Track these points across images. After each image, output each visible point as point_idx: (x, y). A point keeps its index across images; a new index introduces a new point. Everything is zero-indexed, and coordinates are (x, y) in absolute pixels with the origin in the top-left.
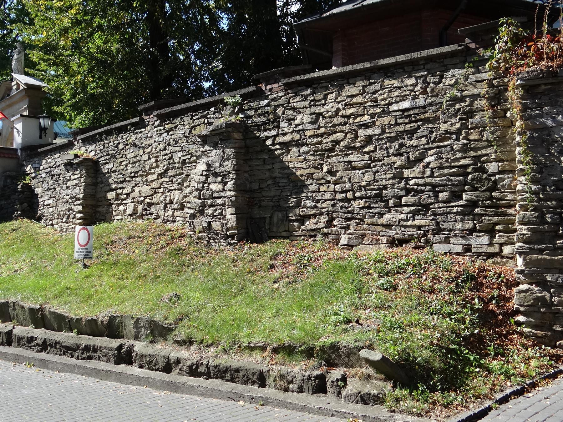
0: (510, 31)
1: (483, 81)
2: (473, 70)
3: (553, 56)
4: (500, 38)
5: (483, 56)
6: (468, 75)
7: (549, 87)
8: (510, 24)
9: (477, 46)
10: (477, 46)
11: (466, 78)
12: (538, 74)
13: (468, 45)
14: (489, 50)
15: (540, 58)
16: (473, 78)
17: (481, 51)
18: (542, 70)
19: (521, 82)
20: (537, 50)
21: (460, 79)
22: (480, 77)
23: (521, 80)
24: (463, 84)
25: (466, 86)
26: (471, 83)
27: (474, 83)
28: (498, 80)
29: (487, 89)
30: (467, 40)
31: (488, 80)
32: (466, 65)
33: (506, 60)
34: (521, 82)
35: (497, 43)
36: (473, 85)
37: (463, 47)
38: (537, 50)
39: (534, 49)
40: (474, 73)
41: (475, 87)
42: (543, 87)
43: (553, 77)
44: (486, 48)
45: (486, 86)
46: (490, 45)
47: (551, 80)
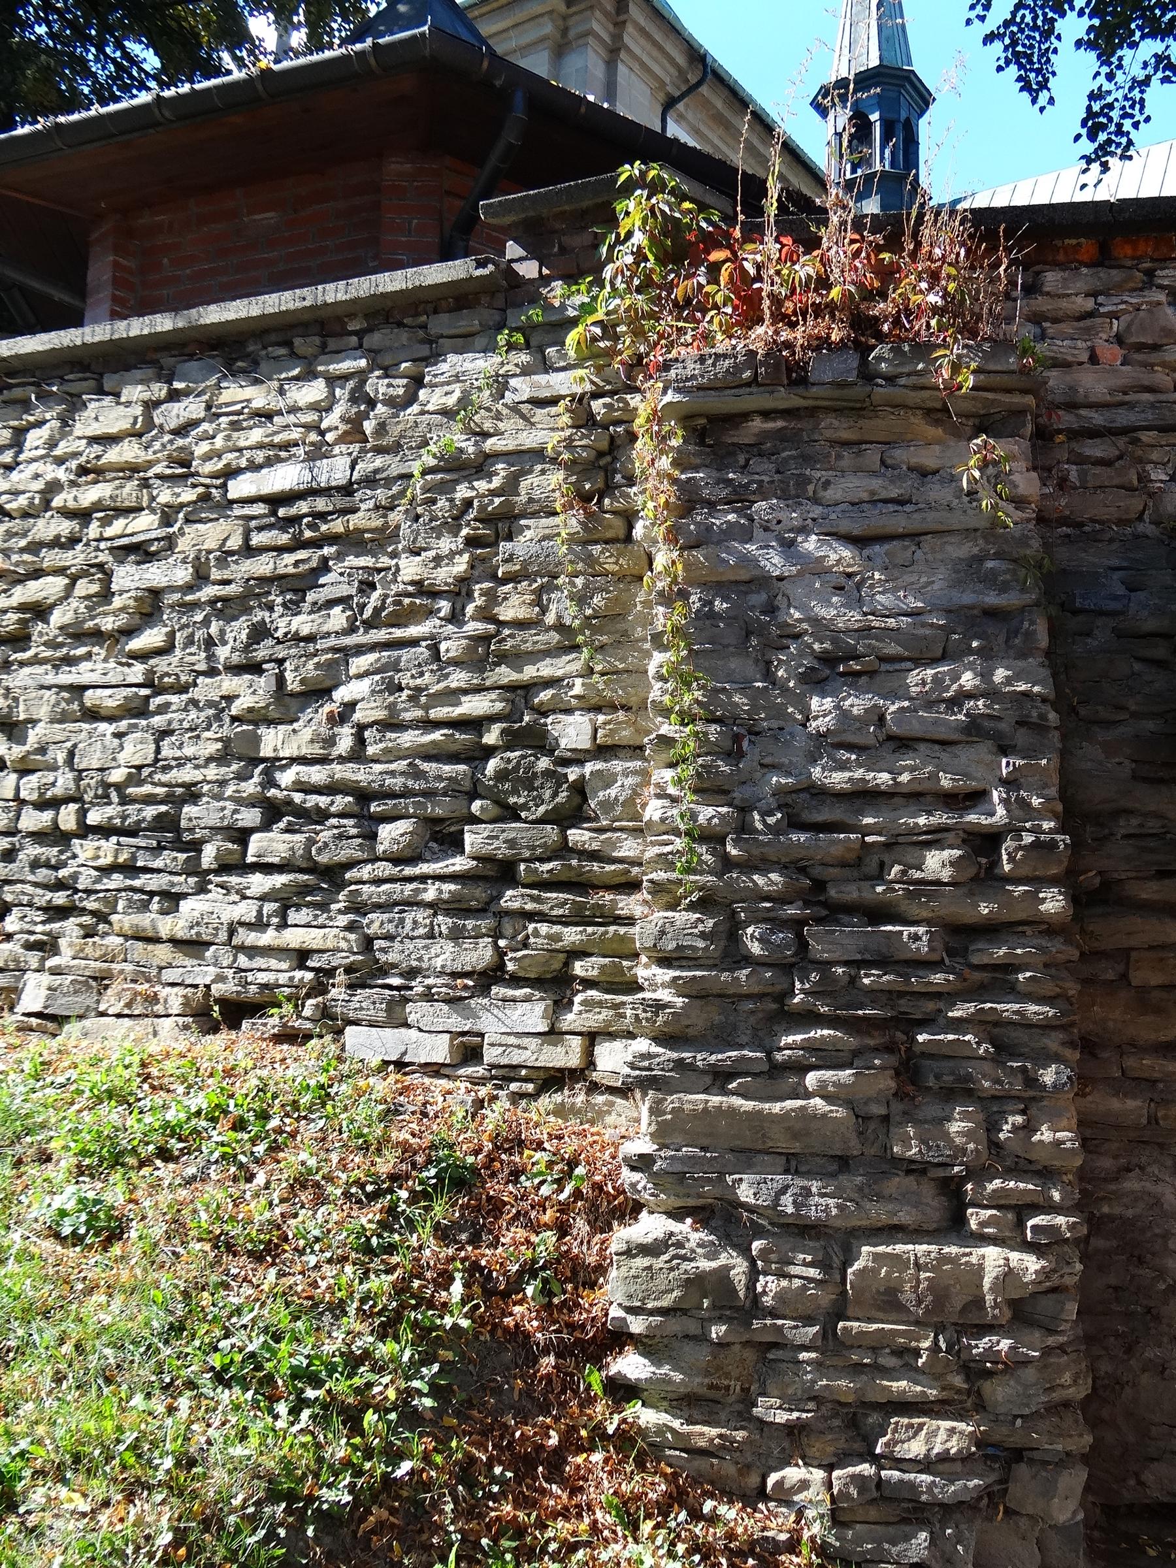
1: (553, 401)
2: (524, 358)
5: (563, 306)
6: (506, 376)
7: (780, 424)
8: (655, 188)
9: (545, 271)
10: (545, 271)
11: (500, 385)
12: (736, 366)
13: (515, 266)
14: (583, 287)
15: (750, 316)
16: (522, 388)
18: (752, 354)
19: (677, 398)
21: (480, 389)
23: (678, 390)
24: (488, 409)
25: (498, 417)
26: (515, 409)
27: (525, 408)
28: (607, 400)
29: (568, 432)
32: (502, 339)
33: (635, 319)
34: (677, 398)
35: (610, 259)
36: (523, 417)
39: (731, 275)
40: (526, 371)
42: (757, 424)
43: (792, 383)
44: (571, 278)
45: (566, 419)
46: (581, 267)
47: (784, 398)
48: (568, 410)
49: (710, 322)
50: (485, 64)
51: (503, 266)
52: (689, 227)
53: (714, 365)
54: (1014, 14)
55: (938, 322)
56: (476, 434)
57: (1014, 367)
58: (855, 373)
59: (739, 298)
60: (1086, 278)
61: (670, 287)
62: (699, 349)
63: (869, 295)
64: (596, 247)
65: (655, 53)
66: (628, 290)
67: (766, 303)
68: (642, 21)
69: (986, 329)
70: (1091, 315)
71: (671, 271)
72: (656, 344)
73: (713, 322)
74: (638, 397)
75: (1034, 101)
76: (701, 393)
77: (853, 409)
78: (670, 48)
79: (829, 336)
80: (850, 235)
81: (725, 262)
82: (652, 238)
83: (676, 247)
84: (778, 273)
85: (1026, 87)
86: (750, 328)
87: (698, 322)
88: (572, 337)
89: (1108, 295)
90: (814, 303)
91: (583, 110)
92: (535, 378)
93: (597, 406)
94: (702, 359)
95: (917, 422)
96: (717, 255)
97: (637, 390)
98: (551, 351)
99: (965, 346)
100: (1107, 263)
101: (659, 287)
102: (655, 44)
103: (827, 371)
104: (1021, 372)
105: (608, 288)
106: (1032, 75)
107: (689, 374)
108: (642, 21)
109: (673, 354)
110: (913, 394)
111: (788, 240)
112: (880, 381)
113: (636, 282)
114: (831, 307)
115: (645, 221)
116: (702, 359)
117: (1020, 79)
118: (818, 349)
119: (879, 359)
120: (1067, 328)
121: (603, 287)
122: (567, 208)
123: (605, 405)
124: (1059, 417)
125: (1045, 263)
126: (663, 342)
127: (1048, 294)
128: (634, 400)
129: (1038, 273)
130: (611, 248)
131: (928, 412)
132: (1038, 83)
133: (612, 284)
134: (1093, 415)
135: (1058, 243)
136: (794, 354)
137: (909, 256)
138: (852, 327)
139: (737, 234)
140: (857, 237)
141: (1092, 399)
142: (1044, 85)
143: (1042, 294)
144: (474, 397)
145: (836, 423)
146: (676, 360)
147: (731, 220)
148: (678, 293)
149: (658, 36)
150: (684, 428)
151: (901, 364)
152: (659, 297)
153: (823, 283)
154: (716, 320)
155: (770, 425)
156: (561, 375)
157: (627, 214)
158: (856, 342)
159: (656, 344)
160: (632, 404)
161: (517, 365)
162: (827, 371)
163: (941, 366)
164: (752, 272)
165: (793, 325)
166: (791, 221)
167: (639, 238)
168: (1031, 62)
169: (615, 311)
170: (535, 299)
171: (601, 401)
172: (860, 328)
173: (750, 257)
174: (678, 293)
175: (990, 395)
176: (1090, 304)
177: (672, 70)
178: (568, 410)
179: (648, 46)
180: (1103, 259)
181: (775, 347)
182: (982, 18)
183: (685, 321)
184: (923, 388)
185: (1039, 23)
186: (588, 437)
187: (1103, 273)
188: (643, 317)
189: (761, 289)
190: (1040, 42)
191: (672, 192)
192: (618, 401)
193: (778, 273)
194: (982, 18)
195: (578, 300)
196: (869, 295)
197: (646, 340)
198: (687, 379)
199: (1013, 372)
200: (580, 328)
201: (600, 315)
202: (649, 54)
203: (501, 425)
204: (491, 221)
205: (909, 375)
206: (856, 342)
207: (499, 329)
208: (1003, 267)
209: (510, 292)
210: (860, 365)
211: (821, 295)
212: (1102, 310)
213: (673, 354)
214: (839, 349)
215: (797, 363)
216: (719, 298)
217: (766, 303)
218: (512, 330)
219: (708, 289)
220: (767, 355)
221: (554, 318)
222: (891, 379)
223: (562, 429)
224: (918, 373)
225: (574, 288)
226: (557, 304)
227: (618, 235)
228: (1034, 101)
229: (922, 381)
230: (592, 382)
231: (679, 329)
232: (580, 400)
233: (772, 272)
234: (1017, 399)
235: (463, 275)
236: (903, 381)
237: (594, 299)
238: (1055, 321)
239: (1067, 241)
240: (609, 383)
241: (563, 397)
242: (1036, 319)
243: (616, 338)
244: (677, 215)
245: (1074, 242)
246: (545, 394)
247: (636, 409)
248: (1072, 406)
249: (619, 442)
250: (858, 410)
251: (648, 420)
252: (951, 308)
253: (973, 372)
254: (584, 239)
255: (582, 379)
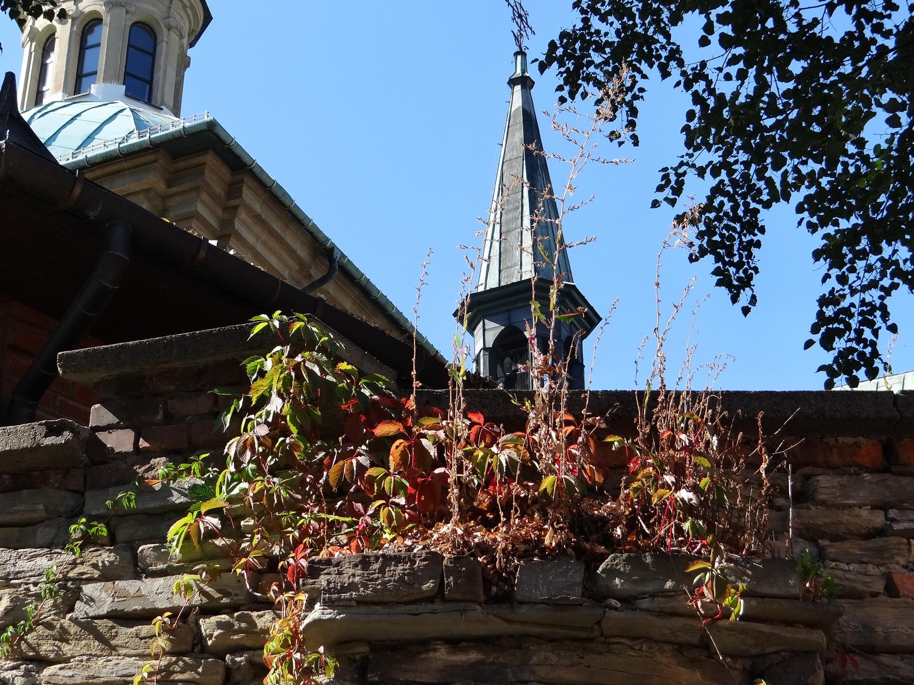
0: (297, 367)
1: (146, 616)
2: (106, 557)
3: (493, 507)
4: (250, 409)
5: (166, 491)
6: (80, 580)
7: (473, 656)
8: (301, 343)
9: (143, 444)
10: (143, 444)
11: (69, 592)
12: (413, 573)
13: (101, 436)
14: (195, 466)
15: (429, 506)
16: (100, 597)
17: (161, 466)
18: (435, 558)
19: (329, 614)
20: (419, 464)
21: (38, 597)
22: (139, 596)
23: (329, 604)
24: (49, 626)
25: (63, 636)
26: (88, 626)
27: (103, 625)
28: (224, 618)
29: (164, 661)
30: (99, 415)
31: (174, 611)
32: (76, 530)
33: (269, 514)
34: (329, 614)
35: (235, 431)
36: (99, 637)
37: (67, 435)
38: (419, 464)
39: (403, 455)
40: (108, 575)
41: (110, 648)
42: (442, 655)
43: (492, 600)
44: (179, 454)
45: (162, 642)
46: (198, 440)
47: (480, 621)
48: (165, 629)
49: (375, 516)
50: (77, 191)
51: (84, 435)
52: (346, 393)
53: (382, 570)
54: (710, 199)
55: (693, 525)
56: (27, 660)
57: (796, 591)
58: (579, 590)
59: (414, 485)
60: (869, 486)
61: (320, 467)
62: (358, 549)
63: (593, 492)
64: (216, 415)
65: (272, 243)
66: (259, 471)
67: (454, 493)
68: (257, 207)
69: (751, 542)
70: (881, 532)
71: (320, 449)
72: (297, 542)
73: (379, 514)
74: (268, 615)
75: (735, 299)
76: (363, 609)
77: (575, 639)
78: (289, 238)
79: (540, 540)
80: (563, 415)
81: (393, 438)
82: (295, 404)
83: (327, 418)
84: (469, 455)
85: (724, 280)
86: (430, 527)
87: (358, 515)
88: (176, 530)
89: (901, 509)
90: (518, 496)
91: (202, 254)
92: (120, 584)
93: (208, 625)
94: (365, 563)
95: (665, 659)
96: (384, 429)
97: (269, 605)
98: (146, 549)
99: (729, 560)
100: (895, 469)
101: (302, 468)
102: (272, 232)
103: (537, 586)
104: (805, 599)
105: (232, 468)
106: (732, 270)
107: (347, 581)
108: (257, 207)
109: (323, 555)
110: (659, 622)
111: (478, 418)
112: (614, 602)
113: (270, 461)
114: (543, 503)
115: (287, 382)
116: (365, 563)
117: (716, 272)
118: (526, 556)
119: (612, 572)
120: (853, 548)
121: (223, 467)
122: (177, 365)
123: (220, 625)
124: (856, 664)
125: (816, 465)
126: (307, 540)
127: (823, 503)
128: (263, 619)
129: (807, 477)
130: (237, 417)
131: (680, 648)
132: (739, 279)
133: (238, 462)
134: (898, 663)
135: (832, 441)
136: (493, 560)
137: (643, 441)
138: (571, 528)
139: (412, 404)
140: (571, 418)
141: (895, 642)
142: (746, 282)
143: (816, 503)
144: (30, 608)
145: (554, 658)
146: (328, 562)
147: (404, 386)
148: (330, 476)
149: (276, 226)
150: (337, 657)
151: (642, 581)
152: (303, 482)
153: (531, 474)
154: (383, 514)
155: (460, 658)
156: (159, 582)
157: (262, 374)
158: (578, 548)
159: (297, 542)
160: (261, 623)
161: (95, 566)
162: (537, 586)
163: (701, 583)
164: (433, 452)
165: (490, 525)
166: (481, 395)
167: (275, 404)
168: (731, 255)
169: (239, 499)
170: (126, 479)
171: (214, 619)
172: (582, 531)
173: (430, 432)
174: (330, 476)
175: (765, 628)
176: (879, 519)
177: (292, 263)
178: (165, 629)
179: (264, 236)
180: (889, 463)
181: (466, 552)
182: (672, 202)
183: (339, 512)
184: (674, 614)
185: (740, 213)
186: (193, 668)
187: (892, 481)
188: (280, 507)
189: (445, 476)
190: (740, 234)
191: (323, 350)
192: (239, 619)
193: (469, 455)
194: (672, 202)
195: (186, 482)
196: (593, 492)
197: (284, 536)
198: (344, 589)
199: (795, 598)
200: (189, 519)
201: (219, 500)
202: (264, 244)
203: (66, 649)
204: (72, 377)
205: (653, 595)
206: (578, 548)
207: (73, 517)
208: (764, 465)
209: (93, 468)
210: (585, 579)
211: (527, 488)
212: (896, 527)
213: (323, 555)
214: (557, 557)
215: (498, 573)
216: (388, 484)
217: (454, 493)
218: (91, 518)
219: (373, 472)
220: (456, 560)
221: (152, 504)
222: (628, 601)
223: (156, 657)
224: (665, 594)
225: (182, 467)
226: (157, 486)
227: (248, 400)
228: (735, 299)
229: (671, 604)
230: (203, 592)
231: (332, 524)
232: (184, 619)
233: (459, 453)
234: (801, 635)
235: (27, 443)
236: (645, 603)
237: (212, 482)
238: (836, 538)
239: (841, 439)
240: (226, 594)
241: (161, 612)
242: (808, 533)
243: (240, 534)
244: (330, 378)
245: (850, 440)
246: (136, 606)
247: (266, 631)
248: (871, 651)
249: (238, 677)
250: (583, 641)
251: (285, 645)
252: (707, 509)
253: (743, 595)
254: (203, 404)
255: (188, 588)
